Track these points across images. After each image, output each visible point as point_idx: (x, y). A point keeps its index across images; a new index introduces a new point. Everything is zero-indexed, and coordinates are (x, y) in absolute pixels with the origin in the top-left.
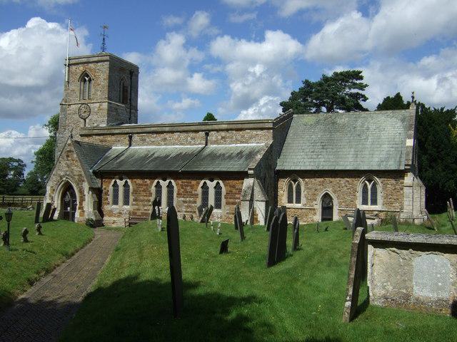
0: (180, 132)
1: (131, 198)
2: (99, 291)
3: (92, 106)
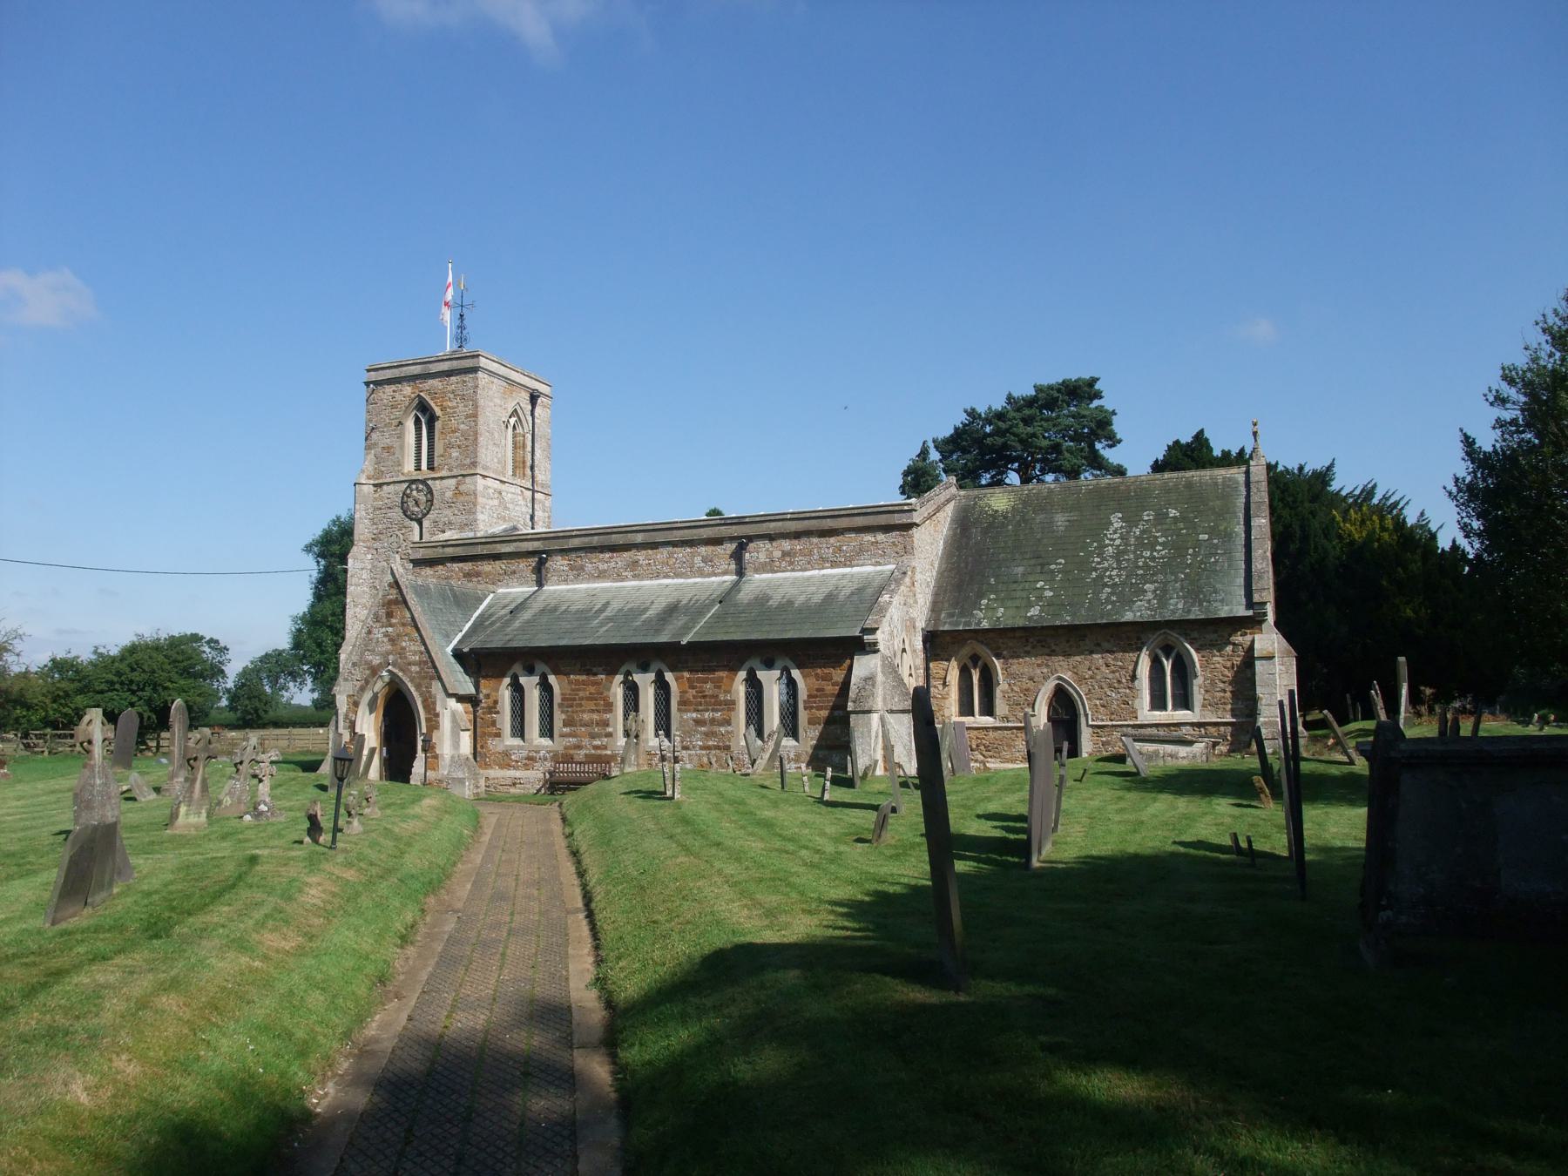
0: (674, 544)
1: (559, 718)
2: (721, 950)
3: (436, 486)
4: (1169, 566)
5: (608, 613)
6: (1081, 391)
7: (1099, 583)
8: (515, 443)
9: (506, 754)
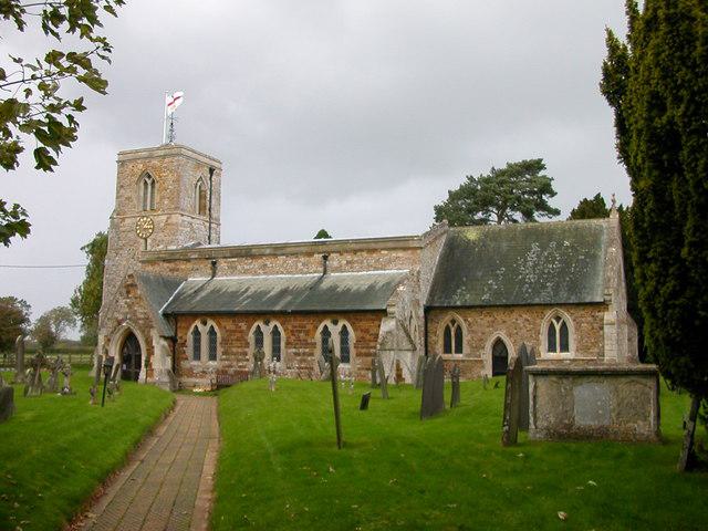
1: (220, 350)
4: (562, 272)
5: (249, 293)
6: (534, 166)
7: (522, 282)
8: (200, 196)
9: (191, 369)
